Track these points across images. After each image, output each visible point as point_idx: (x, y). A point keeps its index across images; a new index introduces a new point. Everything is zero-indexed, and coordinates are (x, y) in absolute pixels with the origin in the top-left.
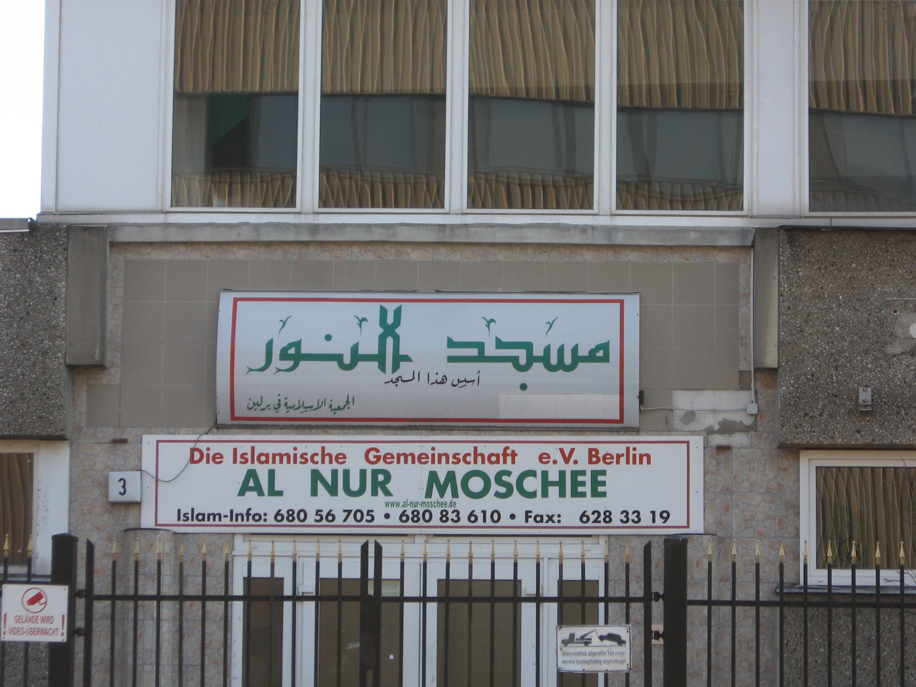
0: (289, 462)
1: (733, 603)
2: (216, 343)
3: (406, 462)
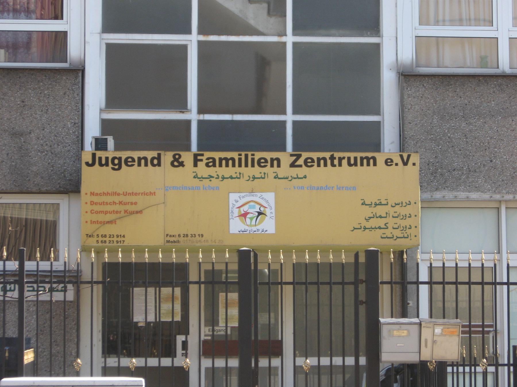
0: (234, 165)
1: (456, 283)
2: (323, 36)
3: (368, 164)
